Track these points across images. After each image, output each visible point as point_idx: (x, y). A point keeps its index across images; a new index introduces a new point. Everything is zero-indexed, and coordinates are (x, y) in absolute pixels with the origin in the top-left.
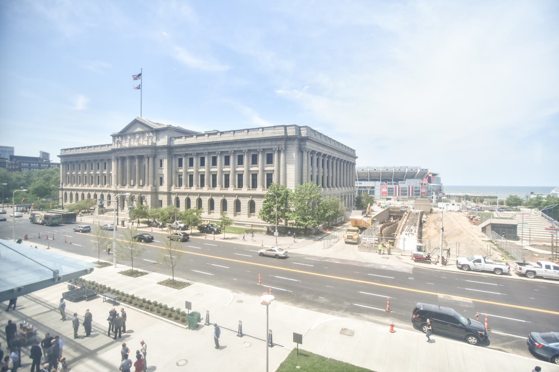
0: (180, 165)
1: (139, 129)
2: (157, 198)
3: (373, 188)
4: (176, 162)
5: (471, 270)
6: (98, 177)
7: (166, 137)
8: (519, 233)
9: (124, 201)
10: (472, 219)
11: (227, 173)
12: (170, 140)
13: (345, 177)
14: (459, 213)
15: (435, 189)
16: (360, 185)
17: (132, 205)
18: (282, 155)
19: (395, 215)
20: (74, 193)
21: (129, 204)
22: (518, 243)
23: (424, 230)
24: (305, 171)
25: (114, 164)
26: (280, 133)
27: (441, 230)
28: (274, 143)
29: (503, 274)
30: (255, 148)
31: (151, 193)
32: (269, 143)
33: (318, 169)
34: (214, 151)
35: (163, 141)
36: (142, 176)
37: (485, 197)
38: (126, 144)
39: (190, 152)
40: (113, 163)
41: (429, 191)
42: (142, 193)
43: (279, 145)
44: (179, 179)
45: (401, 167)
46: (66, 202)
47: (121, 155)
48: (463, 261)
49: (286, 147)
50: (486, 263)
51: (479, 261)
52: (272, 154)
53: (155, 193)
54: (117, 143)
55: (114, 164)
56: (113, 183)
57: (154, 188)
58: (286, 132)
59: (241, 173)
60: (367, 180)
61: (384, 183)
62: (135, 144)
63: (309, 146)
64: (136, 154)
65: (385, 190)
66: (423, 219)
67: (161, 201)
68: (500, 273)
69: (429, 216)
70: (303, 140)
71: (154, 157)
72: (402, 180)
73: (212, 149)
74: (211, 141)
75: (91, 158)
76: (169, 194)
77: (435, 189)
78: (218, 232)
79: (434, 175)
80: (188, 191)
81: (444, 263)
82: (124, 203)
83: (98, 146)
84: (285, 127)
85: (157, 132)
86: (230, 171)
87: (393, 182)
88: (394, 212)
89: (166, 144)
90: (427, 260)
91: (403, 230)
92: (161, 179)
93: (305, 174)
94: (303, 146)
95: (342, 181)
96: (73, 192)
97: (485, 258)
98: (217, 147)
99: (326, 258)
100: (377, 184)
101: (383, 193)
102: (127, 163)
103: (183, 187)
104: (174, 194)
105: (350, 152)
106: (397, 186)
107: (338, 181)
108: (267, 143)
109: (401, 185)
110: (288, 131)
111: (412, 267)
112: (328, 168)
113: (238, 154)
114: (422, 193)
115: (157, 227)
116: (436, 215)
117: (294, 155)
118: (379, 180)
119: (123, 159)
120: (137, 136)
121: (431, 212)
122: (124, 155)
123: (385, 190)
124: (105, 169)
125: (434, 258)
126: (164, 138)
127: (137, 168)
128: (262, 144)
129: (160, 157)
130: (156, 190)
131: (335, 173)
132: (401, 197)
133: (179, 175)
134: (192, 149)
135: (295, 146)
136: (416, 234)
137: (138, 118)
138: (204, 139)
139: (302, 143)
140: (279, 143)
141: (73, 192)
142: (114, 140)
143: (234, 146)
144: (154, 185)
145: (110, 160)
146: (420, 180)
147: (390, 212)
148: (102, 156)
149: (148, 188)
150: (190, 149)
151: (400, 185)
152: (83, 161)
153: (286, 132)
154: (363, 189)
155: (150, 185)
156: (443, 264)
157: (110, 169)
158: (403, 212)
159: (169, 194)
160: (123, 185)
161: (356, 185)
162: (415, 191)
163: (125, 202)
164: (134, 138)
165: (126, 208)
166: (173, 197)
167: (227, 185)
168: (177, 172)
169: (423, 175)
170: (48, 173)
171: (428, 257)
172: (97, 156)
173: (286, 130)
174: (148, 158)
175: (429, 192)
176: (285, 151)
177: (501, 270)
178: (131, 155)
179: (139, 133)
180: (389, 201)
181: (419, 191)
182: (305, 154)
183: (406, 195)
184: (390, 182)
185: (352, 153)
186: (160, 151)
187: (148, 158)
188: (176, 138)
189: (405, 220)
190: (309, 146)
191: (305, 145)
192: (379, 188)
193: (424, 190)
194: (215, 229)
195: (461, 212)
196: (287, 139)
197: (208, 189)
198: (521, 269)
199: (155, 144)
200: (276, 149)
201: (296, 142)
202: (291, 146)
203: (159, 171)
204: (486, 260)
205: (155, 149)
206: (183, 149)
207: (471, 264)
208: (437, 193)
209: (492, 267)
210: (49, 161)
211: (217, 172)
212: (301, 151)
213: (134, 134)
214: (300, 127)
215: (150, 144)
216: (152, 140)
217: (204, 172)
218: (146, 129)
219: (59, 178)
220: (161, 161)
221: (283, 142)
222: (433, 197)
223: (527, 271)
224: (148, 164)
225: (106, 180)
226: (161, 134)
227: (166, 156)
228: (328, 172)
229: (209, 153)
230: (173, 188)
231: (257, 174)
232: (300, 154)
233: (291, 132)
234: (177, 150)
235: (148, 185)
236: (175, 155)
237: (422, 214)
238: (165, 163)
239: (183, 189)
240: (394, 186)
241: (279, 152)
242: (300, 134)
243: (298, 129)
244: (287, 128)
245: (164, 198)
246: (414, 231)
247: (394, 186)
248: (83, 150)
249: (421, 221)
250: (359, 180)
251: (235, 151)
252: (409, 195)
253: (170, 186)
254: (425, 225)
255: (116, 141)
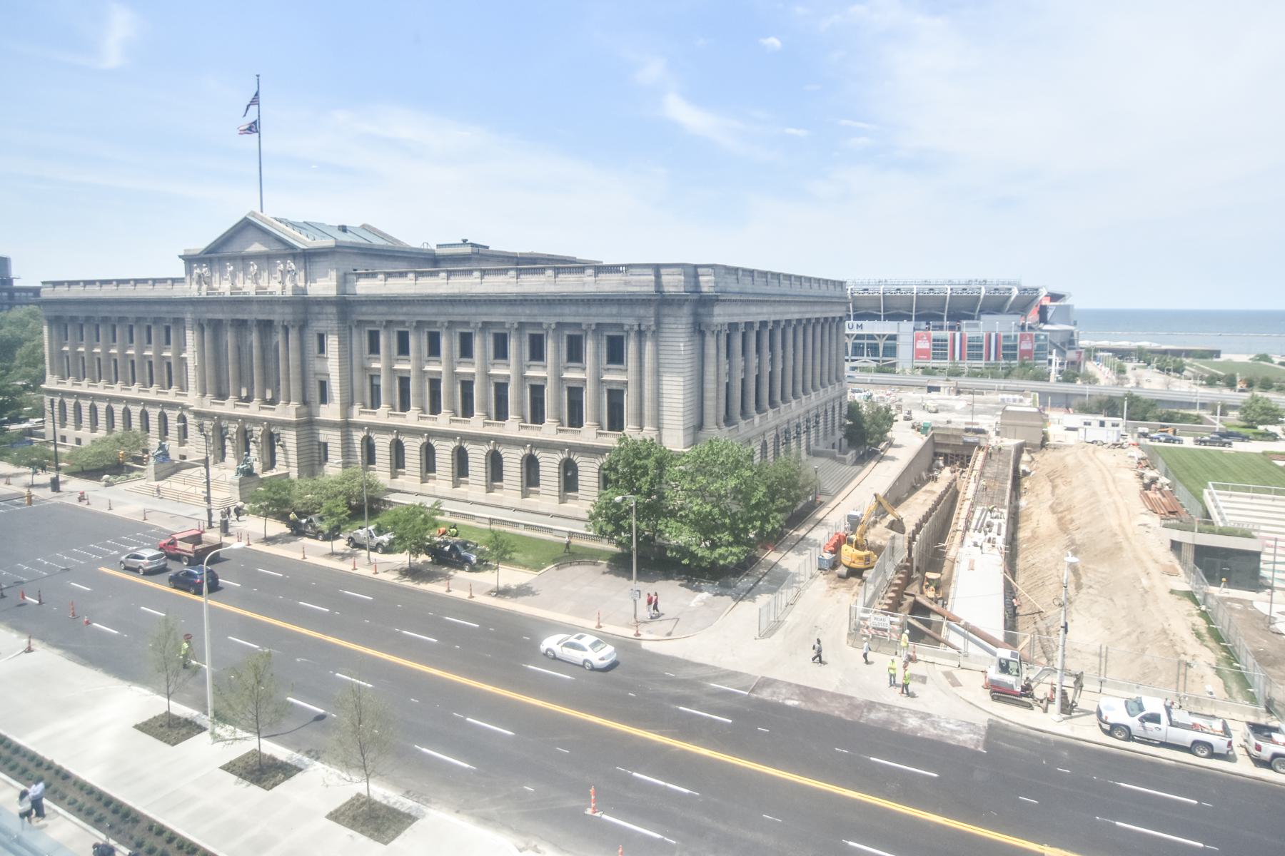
0: (374, 348)
1: (256, 247)
2: (312, 436)
3: (893, 337)
4: (360, 341)
5: (1134, 740)
6: (150, 363)
7: (333, 274)
8: (1265, 572)
9: (223, 440)
10: (1147, 487)
11: (501, 381)
12: (344, 280)
13: (818, 356)
14: (1117, 450)
15: (1057, 340)
16: (860, 332)
17: (246, 461)
18: (649, 347)
19: (948, 451)
20: (85, 405)
21: (238, 456)
22: (1259, 601)
23: (1023, 502)
24: (710, 386)
25: (191, 337)
26: (642, 284)
27: (1062, 632)
28: (626, 310)
29: (1213, 755)
30: (577, 320)
31: (297, 425)
32: (614, 310)
33: (746, 361)
34: (466, 319)
35: (324, 285)
36: (270, 379)
37: (1188, 353)
38: (223, 287)
39: (401, 318)
40: (189, 334)
41: (1040, 348)
42: (271, 423)
43: (640, 318)
44: (372, 385)
45: (969, 282)
46: (63, 425)
47: (210, 316)
48: (1117, 715)
49: (658, 324)
50: (1172, 724)
51: (1155, 718)
52: (621, 338)
53: (308, 425)
54: (199, 283)
55: (191, 337)
56: (192, 385)
57: (304, 410)
58: (658, 282)
59: (539, 383)
60: (877, 317)
61: (923, 325)
62: (248, 288)
63: (721, 316)
64: (253, 317)
65: (924, 345)
66: (1023, 467)
67: (325, 445)
68: (1206, 753)
69: (1037, 456)
70: (701, 303)
71: (303, 327)
72: (971, 318)
73: (459, 313)
74: (456, 291)
75: (131, 313)
76: (346, 427)
77: (1057, 340)
78: (481, 566)
79: (1055, 297)
80: (396, 421)
81: (1068, 708)
82: (224, 447)
83: (145, 281)
84: (657, 268)
85: (308, 257)
86: (508, 377)
87: (946, 323)
88: (947, 445)
89: (332, 293)
90: (1022, 696)
91: (967, 528)
92: (323, 386)
93: (710, 404)
94: (707, 320)
95: (809, 376)
96: (81, 402)
97: (1168, 709)
98: (472, 310)
99: (766, 683)
100: (904, 330)
101: (919, 353)
102: (229, 338)
103: (384, 409)
104: (360, 426)
105: (831, 291)
106: (958, 334)
107: (800, 378)
108: (607, 310)
109: (969, 330)
110: (665, 279)
111: (982, 721)
112: (772, 348)
113: (529, 331)
114: (1024, 352)
115: (316, 538)
116: (1056, 453)
117: (679, 344)
118: (909, 318)
119: (217, 325)
120: (254, 268)
121: (1043, 444)
122: (220, 316)
123: (924, 345)
124: (168, 342)
125: (1040, 691)
126: (326, 275)
127: (255, 352)
128: (594, 310)
129: (317, 326)
130: (310, 414)
131: (790, 363)
132: (966, 365)
133: (372, 377)
134: (405, 309)
135: (684, 320)
136: (1000, 541)
137: (254, 214)
138: (438, 285)
139: (701, 310)
140: (641, 311)
141: (81, 402)
142: (189, 271)
143: (520, 310)
144: (305, 402)
145: (179, 322)
146: (1017, 317)
147: (936, 445)
148: (157, 308)
149: (287, 411)
150: (399, 310)
151: (964, 330)
152: (105, 320)
153: (658, 282)
154: (865, 342)
155: (294, 405)
156: (1063, 711)
157: (182, 347)
158: (971, 446)
159: (346, 427)
160: (221, 395)
161: (848, 331)
162: (1005, 347)
163: (227, 443)
164: (245, 271)
165: (230, 460)
166: (358, 436)
167: (502, 414)
168: (365, 369)
169: (1025, 303)
170: (11, 323)
171: (1027, 690)
172: (142, 308)
173: (658, 276)
174: (286, 330)
175: (1041, 351)
176: (657, 333)
177: (1209, 746)
178: (239, 316)
179: (256, 257)
180: (934, 395)
181: (1014, 348)
182: (711, 342)
183: (979, 357)
184: (937, 323)
185: (838, 292)
186: (316, 309)
187: (286, 330)
188: (359, 276)
189: (978, 466)
190: (721, 316)
191: (711, 315)
192: (910, 339)
193: (1026, 346)
194: (474, 558)
195: (1121, 446)
196: (661, 302)
197: (451, 421)
198: (1258, 748)
199: (304, 291)
200: (631, 326)
201: (686, 310)
202: (672, 320)
203: (317, 365)
204: (1175, 717)
205: (304, 307)
206: (380, 309)
207: (1134, 723)
208: (1062, 352)
209: (1188, 737)
210: (10, 281)
211: (473, 375)
212: (699, 330)
213: (246, 259)
214: (696, 267)
215: (289, 293)
216: (293, 280)
217: (440, 373)
218: (277, 247)
219: (42, 345)
220: (321, 338)
221: (651, 311)
222: (1050, 362)
223: (1275, 756)
224: (288, 350)
225: (171, 375)
226: (320, 264)
227: (334, 324)
228: (772, 360)
229: (452, 324)
230: (357, 408)
231: (581, 389)
232: (697, 338)
233: (673, 283)
234: (364, 309)
235: (288, 402)
236: (360, 322)
237: (1020, 450)
238: (332, 343)
239: (382, 416)
240: (946, 334)
241: (641, 334)
242: (697, 284)
243: (693, 272)
244: (663, 271)
245: (332, 438)
246: (995, 529)
247: (946, 334)
248: (105, 287)
249: (1016, 470)
250: (857, 317)
251: (521, 324)
252: (988, 358)
253: (347, 405)
254: (1026, 483)
255: (195, 276)
